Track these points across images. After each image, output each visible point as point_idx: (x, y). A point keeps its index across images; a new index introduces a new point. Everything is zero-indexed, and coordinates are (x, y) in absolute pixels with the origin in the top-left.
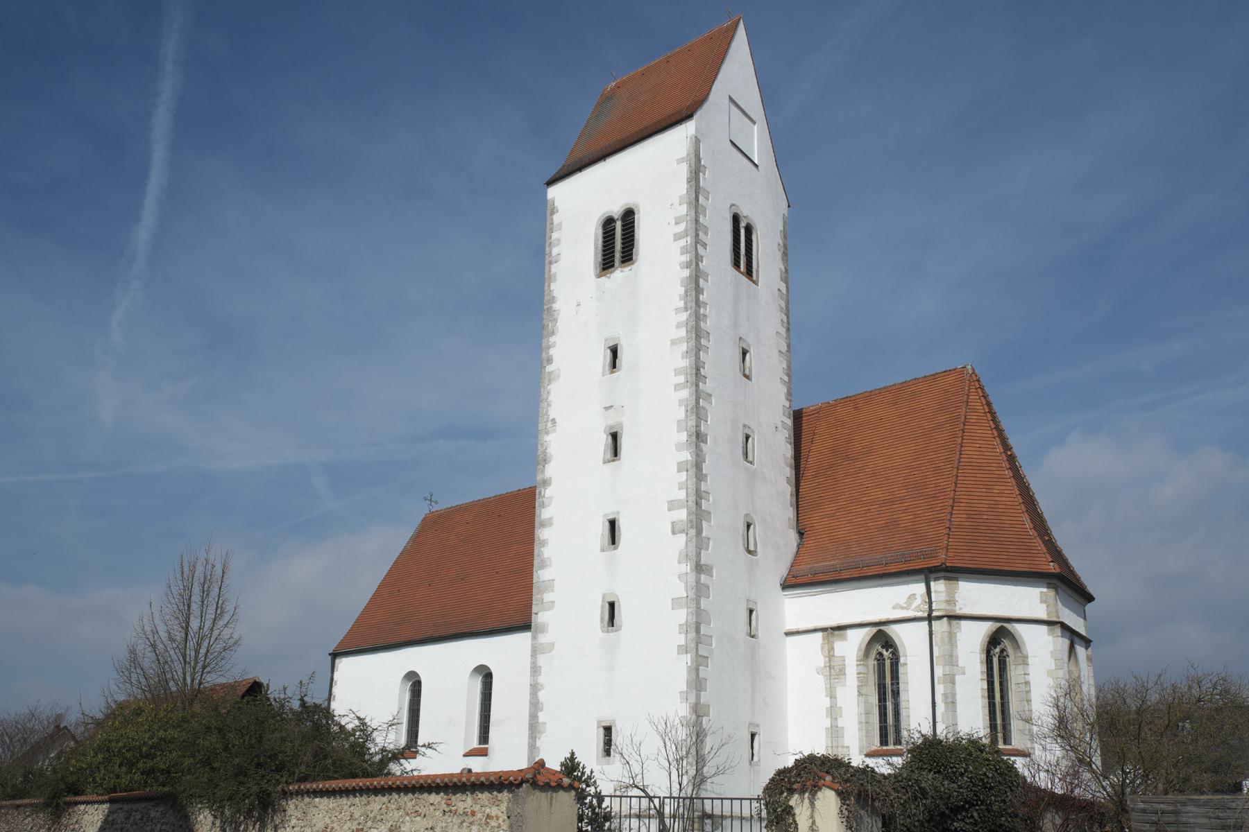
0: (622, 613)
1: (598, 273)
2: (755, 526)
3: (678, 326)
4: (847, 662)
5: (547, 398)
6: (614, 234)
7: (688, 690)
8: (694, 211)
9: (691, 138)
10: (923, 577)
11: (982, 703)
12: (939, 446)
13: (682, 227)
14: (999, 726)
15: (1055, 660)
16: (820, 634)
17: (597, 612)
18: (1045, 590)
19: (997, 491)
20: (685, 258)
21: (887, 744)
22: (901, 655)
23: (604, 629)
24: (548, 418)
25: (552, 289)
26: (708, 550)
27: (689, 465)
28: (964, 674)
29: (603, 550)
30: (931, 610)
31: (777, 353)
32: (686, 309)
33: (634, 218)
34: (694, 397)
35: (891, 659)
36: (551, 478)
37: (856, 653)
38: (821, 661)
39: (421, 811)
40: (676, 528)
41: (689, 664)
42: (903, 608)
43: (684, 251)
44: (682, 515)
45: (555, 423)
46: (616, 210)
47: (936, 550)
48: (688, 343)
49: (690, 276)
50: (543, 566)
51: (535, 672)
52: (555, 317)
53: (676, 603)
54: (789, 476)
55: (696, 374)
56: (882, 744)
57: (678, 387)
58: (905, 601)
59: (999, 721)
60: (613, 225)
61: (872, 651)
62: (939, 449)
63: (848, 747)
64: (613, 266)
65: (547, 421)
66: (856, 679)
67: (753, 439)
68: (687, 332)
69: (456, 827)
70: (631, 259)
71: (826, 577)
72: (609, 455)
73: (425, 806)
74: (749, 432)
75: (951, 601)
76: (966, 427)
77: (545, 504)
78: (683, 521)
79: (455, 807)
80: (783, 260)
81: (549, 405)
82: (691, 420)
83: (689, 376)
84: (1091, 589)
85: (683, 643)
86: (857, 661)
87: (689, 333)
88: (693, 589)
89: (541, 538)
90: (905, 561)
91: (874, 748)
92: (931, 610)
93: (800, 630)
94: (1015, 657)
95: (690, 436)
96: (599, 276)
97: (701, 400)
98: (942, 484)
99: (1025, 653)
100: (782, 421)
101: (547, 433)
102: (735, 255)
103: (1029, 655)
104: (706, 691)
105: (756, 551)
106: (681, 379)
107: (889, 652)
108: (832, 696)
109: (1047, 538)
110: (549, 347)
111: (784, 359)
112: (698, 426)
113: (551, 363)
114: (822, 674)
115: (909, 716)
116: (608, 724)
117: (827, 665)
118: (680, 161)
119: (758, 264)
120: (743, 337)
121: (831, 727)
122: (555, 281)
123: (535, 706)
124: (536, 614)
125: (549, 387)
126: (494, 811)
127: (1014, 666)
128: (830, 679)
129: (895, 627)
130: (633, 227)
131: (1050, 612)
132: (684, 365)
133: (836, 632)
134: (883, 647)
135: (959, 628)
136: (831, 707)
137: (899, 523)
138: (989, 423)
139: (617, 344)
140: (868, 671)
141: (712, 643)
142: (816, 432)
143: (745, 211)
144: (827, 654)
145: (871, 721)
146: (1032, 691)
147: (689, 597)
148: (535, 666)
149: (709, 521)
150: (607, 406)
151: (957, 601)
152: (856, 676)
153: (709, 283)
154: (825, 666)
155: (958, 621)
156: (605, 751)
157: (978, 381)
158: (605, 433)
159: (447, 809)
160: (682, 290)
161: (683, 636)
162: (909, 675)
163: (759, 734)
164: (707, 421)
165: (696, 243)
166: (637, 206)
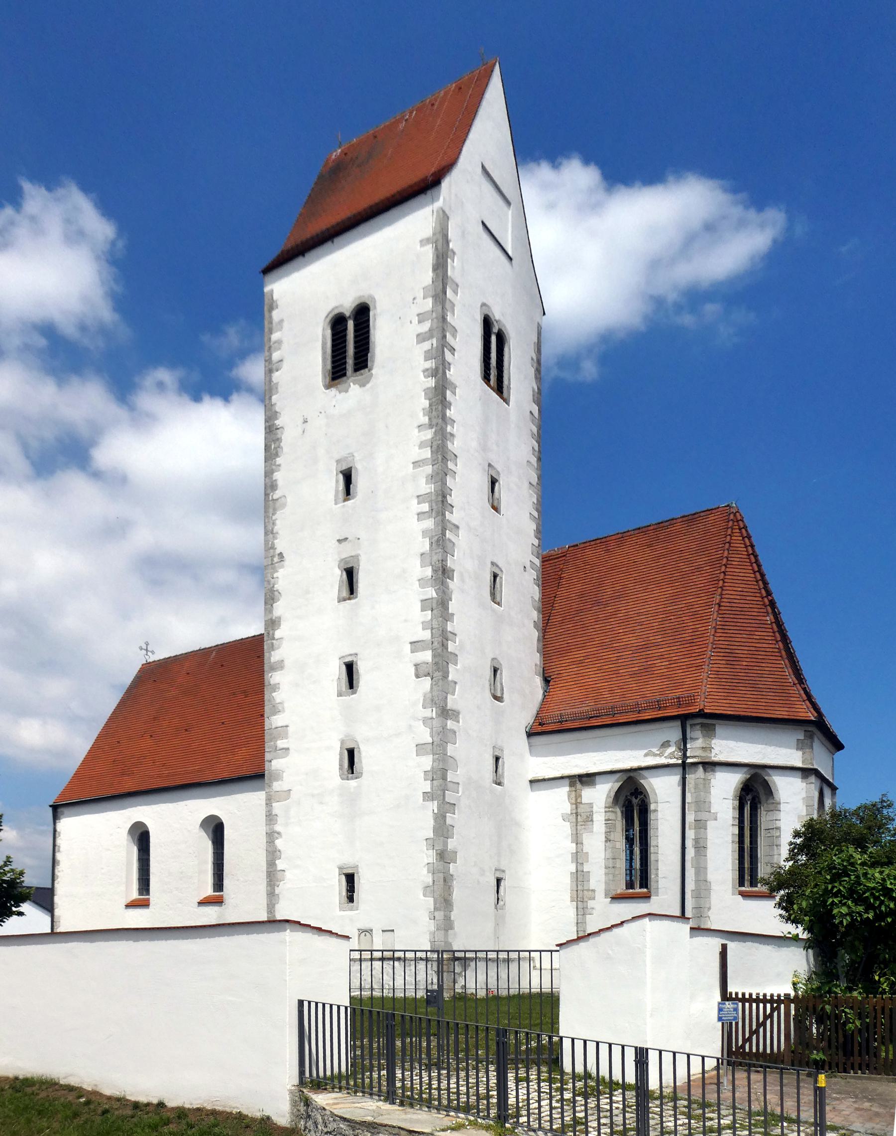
1: (327, 383)
2: (502, 671)
3: (422, 445)
4: (595, 809)
6: (345, 336)
7: (435, 838)
8: (441, 306)
9: (437, 211)
11: (732, 848)
12: (699, 589)
13: (426, 326)
14: (746, 869)
15: (806, 806)
20: (430, 364)
22: (651, 802)
23: (343, 776)
24: (274, 552)
26: (454, 695)
27: (435, 601)
28: (716, 819)
29: (340, 694)
30: (685, 756)
31: (526, 485)
32: (431, 426)
34: (440, 528)
38: (567, 808)
40: (421, 672)
41: (436, 811)
43: (428, 356)
44: (427, 656)
46: (347, 306)
48: (433, 465)
50: (276, 711)
51: (271, 820)
52: (279, 436)
54: (536, 620)
55: (443, 501)
57: (420, 515)
59: (747, 865)
62: (698, 593)
63: (593, 891)
64: (345, 375)
67: (501, 578)
71: (576, 725)
72: (345, 593)
74: (497, 571)
75: (708, 749)
76: (728, 570)
77: (275, 646)
78: (428, 663)
80: (536, 378)
82: (436, 553)
83: (434, 504)
85: (429, 790)
86: (606, 807)
87: (434, 455)
91: (619, 891)
92: (685, 756)
93: (547, 777)
95: (435, 571)
97: (447, 531)
98: (700, 629)
99: (778, 800)
100: (530, 561)
103: (782, 801)
104: (453, 838)
105: (502, 697)
106: (425, 507)
107: (638, 799)
108: (577, 840)
111: (535, 493)
112: (444, 561)
115: (657, 861)
116: (350, 871)
117: (574, 812)
118: (424, 242)
119: (509, 380)
120: (492, 464)
121: (577, 871)
123: (273, 854)
125: (274, 518)
127: (765, 813)
128: (577, 826)
131: (806, 759)
136: (577, 852)
137: (653, 669)
138: (751, 566)
139: (351, 467)
140: (616, 817)
141: (458, 791)
142: (562, 576)
143: (497, 314)
144: (573, 801)
145: (618, 866)
147: (435, 743)
149: (456, 664)
151: (713, 748)
153: (457, 397)
154: (572, 813)
155: (714, 767)
156: (348, 898)
157: (742, 521)
158: (339, 568)
160: (426, 403)
163: (505, 879)
164: (453, 556)
165: (443, 346)
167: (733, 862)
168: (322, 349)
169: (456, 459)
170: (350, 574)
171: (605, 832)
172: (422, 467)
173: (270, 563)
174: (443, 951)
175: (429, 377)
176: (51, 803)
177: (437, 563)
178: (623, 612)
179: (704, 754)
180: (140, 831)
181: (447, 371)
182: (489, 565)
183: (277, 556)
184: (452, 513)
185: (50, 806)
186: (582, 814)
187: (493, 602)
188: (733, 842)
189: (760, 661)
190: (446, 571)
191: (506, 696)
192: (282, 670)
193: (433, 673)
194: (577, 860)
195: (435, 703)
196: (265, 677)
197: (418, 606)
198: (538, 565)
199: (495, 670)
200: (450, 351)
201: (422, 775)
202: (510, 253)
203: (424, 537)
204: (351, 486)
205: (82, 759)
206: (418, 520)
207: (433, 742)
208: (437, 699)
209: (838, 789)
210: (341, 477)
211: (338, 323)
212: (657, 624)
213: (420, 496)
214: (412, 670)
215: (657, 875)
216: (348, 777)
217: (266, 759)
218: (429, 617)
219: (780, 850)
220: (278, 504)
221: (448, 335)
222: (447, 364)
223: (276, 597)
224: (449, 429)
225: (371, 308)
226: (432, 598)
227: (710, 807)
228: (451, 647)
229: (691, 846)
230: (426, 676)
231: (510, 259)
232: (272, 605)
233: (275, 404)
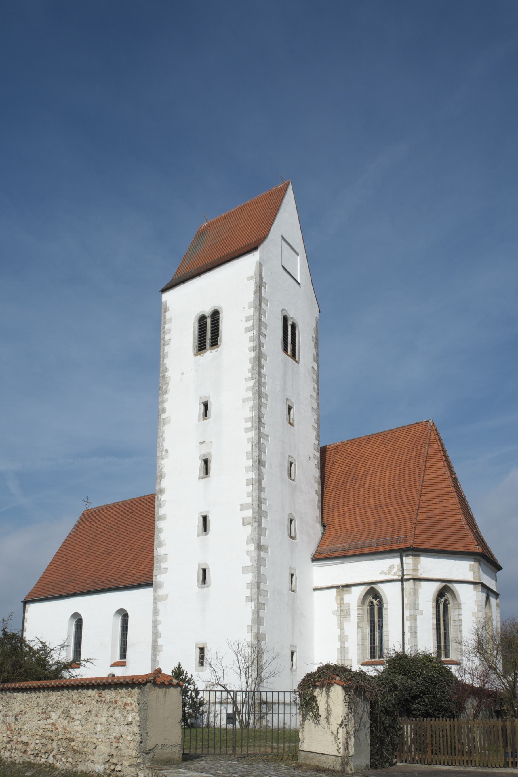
2: (295, 521)
3: (247, 389)
4: (351, 608)
5: (162, 436)
6: (206, 327)
8: (258, 313)
9: (257, 263)
10: (398, 554)
13: (250, 323)
15: (477, 606)
16: (335, 590)
17: (195, 575)
18: (472, 563)
20: (252, 344)
21: (374, 658)
24: (163, 449)
27: (254, 480)
28: (422, 614)
29: (198, 535)
30: (403, 575)
32: (252, 378)
33: (219, 316)
35: (378, 605)
38: (335, 606)
40: (246, 522)
41: (253, 608)
42: (386, 574)
43: (251, 340)
45: (168, 452)
46: (207, 311)
47: (407, 537)
51: (155, 613)
54: (317, 489)
55: (259, 422)
56: (371, 658)
57: (246, 430)
59: (442, 644)
61: (366, 601)
63: (351, 660)
64: (205, 348)
65: (162, 451)
66: (356, 618)
67: (295, 465)
69: (105, 710)
70: (217, 344)
72: (203, 474)
74: (292, 461)
75: (416, 569)
77: (162, 505)
80: (315, 348)
81: (163, 440)
83: (254, 423)
84: (500, 562)
85: (249, 595)
86: (358, 606)
88: (255, 560)
91: (366, 660)
94: (453, 604)
95: (254, 462)
96: (196, 355)
97: (261, 439)
101: (162, 459)
103: (462, 603)
105: (295, 537)
106: (249, 425)
107: (377, 601)
108: (342, 628)
109: (475, 531)
110: (163, 402)
112: (259, 456)
113: (165, 413)
115: (388, 641)
116: (202, 646)
117: (339, 609)
118: (249, 279)
119: (299, 350)
120: (289, 398)
121: (341, 647)
123: (156, 635)
124: (156, 576)
125: (163, 428)
126: (129, 700)
129: (381, 586)
132: (251, 415)
133: (345, 589)
134: (373, 598)
135: (420, 586)
136: (341, 635)
137: (385, 520)
140: (364, 613)
141: (267, 595)
143: (291, 314)
147: (253, 566)
148: (155, 609)
149: (266, 517)
150: (201, 442)
152: (356, 616)
153: (268, 362)
154: (338, 610)
156: (200, 663)
158: (200, 459)
159: (99, 700)
161: (249, 590)
165: (260, 334)
166: (221, 308)
167: (433, 642)
168: (193, 333)
169: (267, 397)
173: (160, 455)
174: (236, 691)
176: (23, 600)
178: (368, 484)
179: (414, 574)
180: (124, 613)
181: (262, 348)
182: (287, 457)
183: (164, 451)
184: (265, 428)
185: (22, 602)
186: (344, 611)
187: (290, 479)
188: (433, 629)
189: (447, 515)
190: (261, 462)
191: (298, 536)
195: (254, 542)
196: (155, 523)
197: (245, 483)
198: (318, 456)
199: (291, 521)
200: (263, 337)
201: (246, 585)
202: (299, 281)
203: (248, 442)
205: (44, 571)
206: (245, 432)
210: (202, 406)
211: (202, 319)
212: (388, 492)
214: (241, 521)
218: (251, 490)
219: (462, 634)
220: (166, 421)
221: (262, 328)
222: (261, 344)
224: (263, 380)
225: (220, 312)
227: (418, 607)
228: (263, 507)
229: (408, 631)
231: (299, 284)
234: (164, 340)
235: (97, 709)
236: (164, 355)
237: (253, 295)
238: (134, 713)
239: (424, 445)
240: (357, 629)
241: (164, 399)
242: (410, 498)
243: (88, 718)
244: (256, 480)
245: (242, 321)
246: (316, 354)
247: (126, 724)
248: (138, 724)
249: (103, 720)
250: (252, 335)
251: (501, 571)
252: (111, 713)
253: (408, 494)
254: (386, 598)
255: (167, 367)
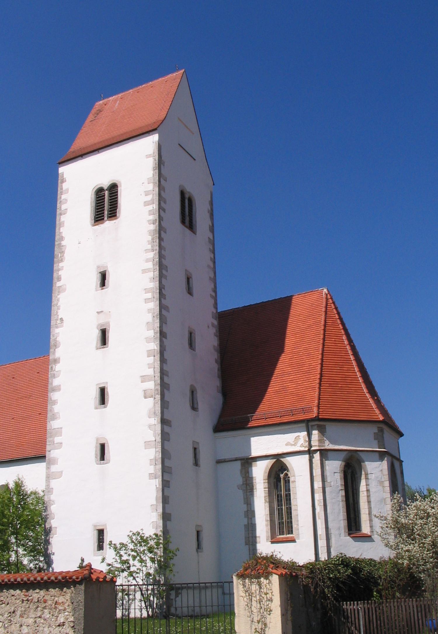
0: (110, 452)
5: (57, 304)
9: (156, 143)
10: (304, 425)
17: (93, 451)
19: (346, 369)
24: (58, 317)
25: (61, 232)
29: (96, 408)
33: (117, 190)
36: (59, 358)
37: (263, 475)
39: (4, 600)
41: (158, 487)
42: (292, 445)
45: (63, 321)
46: (105, 184)
47: (311, 407)
48: (154, 272)
49: (155, 229)
50: (54, 418)
52: (63, 250)
53: (147, 445)
57: (147, 301)
58: (293, 441)
60: (103, 193)
64: (103, 219)
65: (57, 320)
66: (263, 492)
68: (154, 265)
69: (32, 611)
70: (116, 216)
73: (8, 597)
77: (56, 376)
78: (151, 389)
79: (31, 597)
81: (59, 309)
83: (155, 294)
84: (402, 429)
85: (153, 472)
86: (264, 480)
88: (159, 435)
89: (52, 399)
90: (293, 415)
96: (94, 226)
101: (57, 327)
102: (182, 215)
106: (149, 295)
109: (376, 398)
110: (59, 270)
113: (60, 281)
114: (242, 489)
122: (63, 226)
124: (50, 451)
125: (58, 297)
126: (61, 599)
130: (117, 195)
132: (152, 286)
136: (248, 511)
146: (371, 496)
147: (157, 441)
148: (49, 488)
150: (99, 311)
154: (243, 484)
158: (97, 329)
159: (25, 599)
161: (153, 466)
162: (297, 488)
166: (120, 182)
170: (104, 333)
171: (265, 497)
172: (147, 272)
173: (55, 324)
175: (151, 224)
177: (157, 328)
183: (59, 320)
188: (342, 501)
192: (59, 391)
193: (155, 396)
194: (248, 515)
195: (157, 415)
200: (163, 210)
204: (106, 281)
207: (155, 441)
208: (158, 412)
209: (403, 461)
211: (99, 192)
213: (147, 289)
215: (298, 525)
216: (101, 463)
217: (47, 450)
218: (152, 361)
223: (57, 345)
226: (154, 349)
230: (150, 397)
232: (55, 350)
233: (62, 232)
234: (61, 209)
235: (23, 609)
236: (60, 224)
237: (152, 172)
238: (66, 613)
239: (321, 313)
240: (264, 504)
241: (60, 267)
242: (311, 367)
243: (12, 619)
244: (157, 351)
245: (141, 195)
246: (211, 225)
247: (58, 624)
248: (72, 625)
249: (31, 621)
250: (152, 209)
251: (403, 437)
252: (39, 614)
253: (309, 363)
254: (293, 470)
255: (63, 235)
